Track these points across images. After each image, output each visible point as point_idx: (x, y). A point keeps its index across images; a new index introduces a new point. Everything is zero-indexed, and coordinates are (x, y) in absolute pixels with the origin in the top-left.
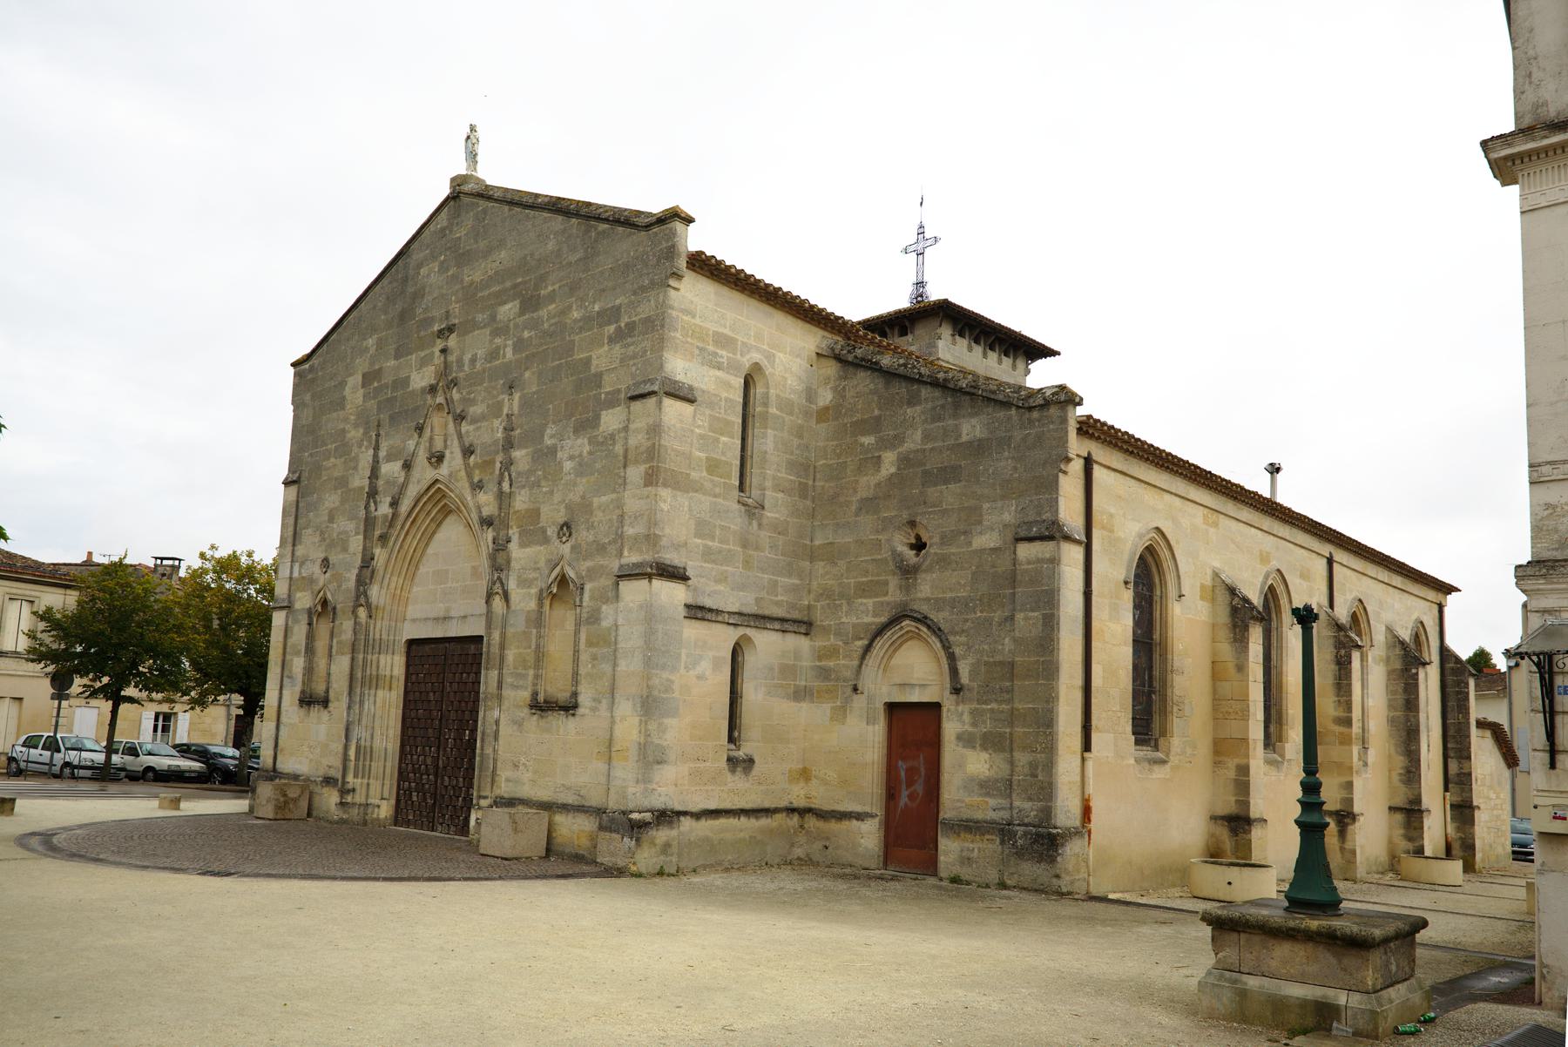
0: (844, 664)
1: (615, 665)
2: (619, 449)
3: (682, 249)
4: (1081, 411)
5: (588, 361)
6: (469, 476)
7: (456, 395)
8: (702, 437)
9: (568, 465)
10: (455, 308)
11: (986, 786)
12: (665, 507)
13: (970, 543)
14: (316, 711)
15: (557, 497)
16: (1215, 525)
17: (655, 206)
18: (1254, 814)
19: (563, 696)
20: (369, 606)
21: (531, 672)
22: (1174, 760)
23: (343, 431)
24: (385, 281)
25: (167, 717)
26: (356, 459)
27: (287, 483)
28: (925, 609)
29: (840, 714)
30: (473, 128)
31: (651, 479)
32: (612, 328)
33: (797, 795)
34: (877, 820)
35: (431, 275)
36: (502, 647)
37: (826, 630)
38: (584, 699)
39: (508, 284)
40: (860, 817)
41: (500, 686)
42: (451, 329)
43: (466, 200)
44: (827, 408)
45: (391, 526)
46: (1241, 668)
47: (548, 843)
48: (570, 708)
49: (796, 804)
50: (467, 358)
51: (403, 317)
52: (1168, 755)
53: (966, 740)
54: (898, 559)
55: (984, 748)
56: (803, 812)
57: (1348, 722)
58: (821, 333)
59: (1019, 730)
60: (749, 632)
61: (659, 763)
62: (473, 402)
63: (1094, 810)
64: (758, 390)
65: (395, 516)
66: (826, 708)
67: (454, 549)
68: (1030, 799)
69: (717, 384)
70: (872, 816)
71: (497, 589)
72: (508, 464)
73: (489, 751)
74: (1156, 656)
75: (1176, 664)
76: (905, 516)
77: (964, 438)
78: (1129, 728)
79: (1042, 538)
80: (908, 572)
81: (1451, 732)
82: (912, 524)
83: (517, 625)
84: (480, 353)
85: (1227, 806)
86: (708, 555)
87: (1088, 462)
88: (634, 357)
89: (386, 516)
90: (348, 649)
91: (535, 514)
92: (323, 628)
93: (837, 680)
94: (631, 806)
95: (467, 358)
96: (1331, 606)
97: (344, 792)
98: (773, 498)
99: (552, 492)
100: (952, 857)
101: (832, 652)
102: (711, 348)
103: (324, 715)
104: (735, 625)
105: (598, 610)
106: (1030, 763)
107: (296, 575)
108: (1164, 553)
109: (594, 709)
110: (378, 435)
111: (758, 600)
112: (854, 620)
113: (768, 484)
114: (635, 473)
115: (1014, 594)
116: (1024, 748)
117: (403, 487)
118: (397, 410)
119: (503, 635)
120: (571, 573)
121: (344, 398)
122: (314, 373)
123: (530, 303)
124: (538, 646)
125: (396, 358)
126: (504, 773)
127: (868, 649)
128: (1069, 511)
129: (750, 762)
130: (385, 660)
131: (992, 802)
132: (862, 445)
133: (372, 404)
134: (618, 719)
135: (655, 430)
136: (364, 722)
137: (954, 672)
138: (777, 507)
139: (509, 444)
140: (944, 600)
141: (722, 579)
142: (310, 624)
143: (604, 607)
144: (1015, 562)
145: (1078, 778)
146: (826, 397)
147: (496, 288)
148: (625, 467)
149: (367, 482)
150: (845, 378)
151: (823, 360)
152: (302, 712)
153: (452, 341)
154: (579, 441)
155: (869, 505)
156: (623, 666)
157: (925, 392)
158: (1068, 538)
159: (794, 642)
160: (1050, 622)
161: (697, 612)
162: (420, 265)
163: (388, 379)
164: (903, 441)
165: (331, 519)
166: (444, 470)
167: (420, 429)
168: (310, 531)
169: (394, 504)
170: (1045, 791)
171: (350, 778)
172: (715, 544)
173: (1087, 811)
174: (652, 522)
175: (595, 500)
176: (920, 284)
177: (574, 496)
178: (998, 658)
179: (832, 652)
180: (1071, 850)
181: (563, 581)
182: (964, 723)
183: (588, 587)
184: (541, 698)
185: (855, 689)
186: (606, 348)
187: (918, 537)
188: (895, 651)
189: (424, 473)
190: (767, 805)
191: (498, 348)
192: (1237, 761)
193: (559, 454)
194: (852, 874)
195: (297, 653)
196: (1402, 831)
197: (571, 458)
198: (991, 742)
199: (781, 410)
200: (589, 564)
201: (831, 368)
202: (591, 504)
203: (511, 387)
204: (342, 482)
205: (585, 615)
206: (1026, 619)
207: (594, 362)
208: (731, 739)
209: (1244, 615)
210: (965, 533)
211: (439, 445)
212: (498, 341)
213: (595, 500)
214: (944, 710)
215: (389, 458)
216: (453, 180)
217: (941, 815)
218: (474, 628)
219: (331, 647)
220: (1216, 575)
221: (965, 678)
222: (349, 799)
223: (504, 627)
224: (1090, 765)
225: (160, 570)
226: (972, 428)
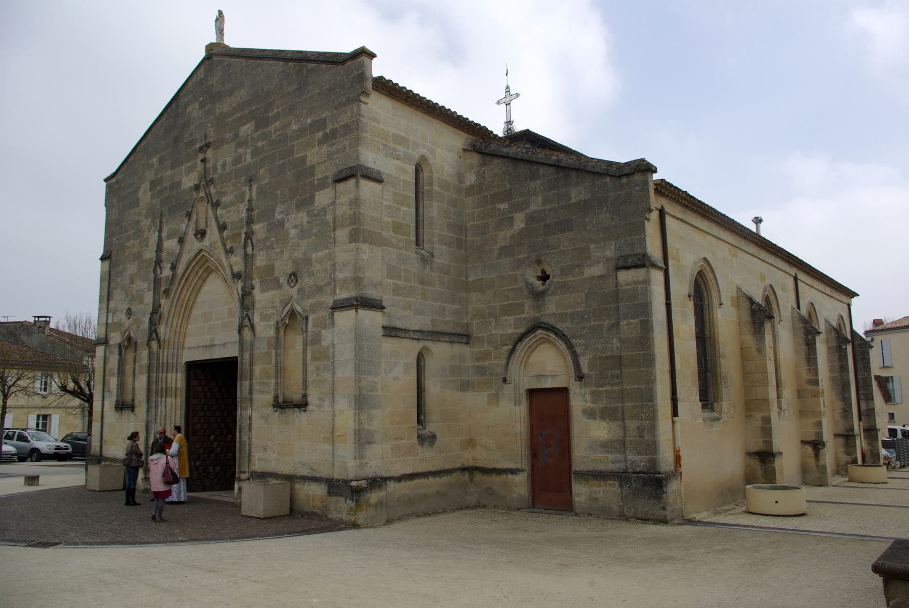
0: (496, 363)
1: (334, 373)
2: (329, 217)
3: (368, 75)
4: (656, 177)
5: (304, 158)
6: (224, 245)
7: (213, 190)
8: (388, 207)
9: (293, 232)
10: (211, 132)
11: (606, 446)
12: (365, 257)
14: (126, 414)
15: (286, 255)
16: (735, 256)
17: (347, 47)
18: (775, 450)
19: (297, 398)
21: (273, 381)
22: (724, 417)
23: (139, 221)
24: (163, 119)
25: (45, 417)
26: (147, 240)
27: (103, 259)
28: (552, 321)
29: (495, 399)
30: (220, 13)
31: (355, 237)
32: (320, 134)
33: (468, 458)
34: (526, 473)
35: (194, 111)
36: (251, 364)
37: (481, 340)
38: (312, 399)
39: (246, 111)
40: (513, 472)
41: (251, 393)
42: (208, 145)
43: (216, 59)
44: (472, 187)
45: (171, 283)
46: (761, 350)
47: (291, 504)
49: (466, 465)
50: (219, 165)
51: (176, 140)
52: (720, 412)
53: (590, 414)
54: (529, 285)
55: (603, 418)
56: (471, 470)
57: (816, 382)
58: (465, 135)
59: (628, 404)
60: (429, 344)
61: (370, 443)
62: (224, 194)
63: (682, 458)
64: (426, 174)
65: (174, 276)
66: (485, 394)
67: (217, 295)
68: (639, 454)
69: (397, 170)
70: (522, 470)
71: (246, 323)
72: (249, 236)
73: (245, 439)
74: (708, 347)
75: (721, 351)
76: (533, 256)
77: (574, 200)
78: (698, 398)
79: (636, 267)
80: (538, 296)
81: (861, 384)
82: (539, 262)
83: (261, 348)
84: (229, 159)
85: (757, 444)
86: (396, 290)
87: (662, 213)
88: (338, 152)
89: (168, 277)
90: (145, 370)
91: (270, 269)
92: (130, 356)
93: (491, 374)
94: (351, 476)
95: (219, 165)
96: (799, 307)
98: (439, 248)
99: (282, 252)
100: (583, 498)
101: (486, 356)
102: (391, 145)
103: (132, 416)
104: (418, 339)
105: (319, 334)
106: (638, 428)
107: (110, 321)
108: (709, 275)
109: (319, 406)
110: (161, 222)
111: (433, 321)
112: (501, 332)
113: (436, 239)
114: (342, 234)
115: (618, 307)
116: (633, 417)
117: (179, 256)
118: (174, 204)
119: (252, 355)
120: (299, 309)
121: (138, 199)
122: (119, 186)
123: (262, 122)
124: (277, 363)
125: (172, 169)
126: (257, 455)
127: (512, 351)
128: (653, 248)
129: (433, 437)
130: (171, 377)
131: (611, 457)
132: (499, 210)
133: (157, 201)
134: (337, 413)
135: (356, 202)
136: (158, 421)
137: (577, 365)
138: (442, 255)
139: (250, 221)
140: (566, 314)
141: (408, 307)
142: (120, 354)
143: (324, 332)
144: (617, 284)
145: (671, 436)
146: (471, 179)
147: (238, 115)
148: (334, 230)
149: (154, 254)
151: (468, 154)
152: (117, 414)
153: (209, 154)
154: (300, 215)
155: (506, 251)
156: (339, 373)
157: (542, 170)
158: (654, 266)
159: (458, 349)
160: (646, 326)
161: (391, 331)
162: (186, 107)
163: (167, 184)
165: (132, 282)
166: (206, 242)
167: (189, 215)
168: (118, 291)
169: (174, 268)
170: (652, 447)
172: (401, 283)
173: (678, 459)
174: (357, 269)
175: (314, 255)
176: (509, 123)
177: (298, 254)
178: (609, 354)
179: (486, 356)
180: (673, 487)
181: (293, 314)
182: (586, 401)
183: (311, 318)
184: (280, 400)
185: (505, 380)
186: (317, 148)
187: (543, 272)
188: (532, 351)
189: (193, 245)
190: (447, 467)
191: (241, 155)
192: (761, 414)
193: (286, 225)
194: (505, 506)
195: (113, 375)
196: (843, 449)
197: (295, 227)
198: (607, 414)
199: (440, 187)
200: (311, 301)
201: (475, 159)
202: (310, 259)
203: (250, 181)
204: (138, 256)
205: (309, 338)
207: (309, 159)
208: (419, 422)
209: (760, 314)
210: (578, 266)
211: (202, 226)
212: (240, 150)
213: (314, 255)
214: (571, 394)
215: (169, 237)
216: (207, 47)
217: (574, 468)
218: (231, 351)
219: (134, 369)
220: (739, 289)
221: (585, 370)
223: (252, 350)
224: (678, 426)
225: (38, 324)
226: (578, 193)
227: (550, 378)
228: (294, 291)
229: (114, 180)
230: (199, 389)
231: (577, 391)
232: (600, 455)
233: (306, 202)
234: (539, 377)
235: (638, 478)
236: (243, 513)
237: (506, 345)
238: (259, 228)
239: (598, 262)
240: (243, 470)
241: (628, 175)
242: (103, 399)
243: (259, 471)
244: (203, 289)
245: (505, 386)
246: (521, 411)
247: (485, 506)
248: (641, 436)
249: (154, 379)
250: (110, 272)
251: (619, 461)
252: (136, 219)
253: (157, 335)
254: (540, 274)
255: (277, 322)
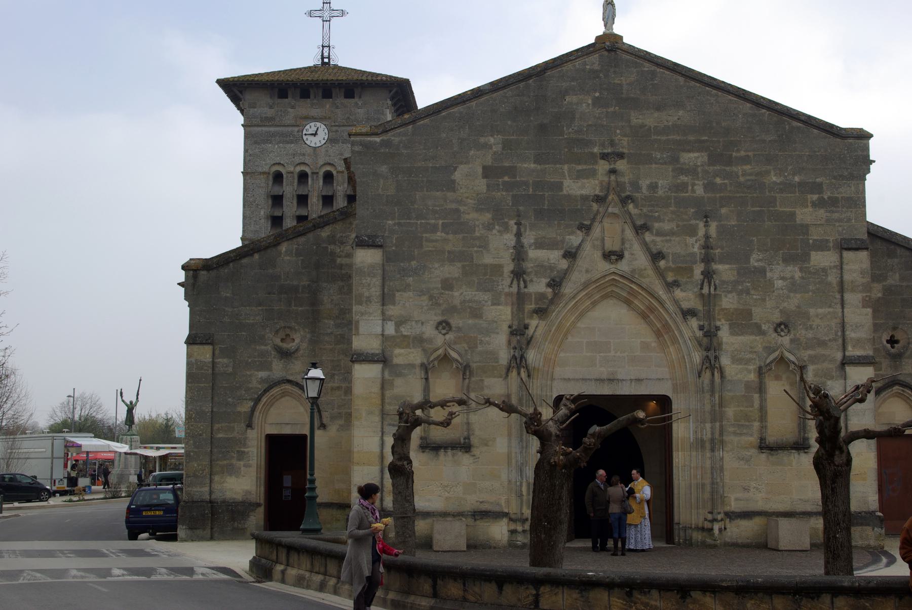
9: (779, 283)
20: (527, 367)
32: (815, 197)
157: (899, 251)
197: (783, 278)
228: (786, 340)
243: (737, 510)
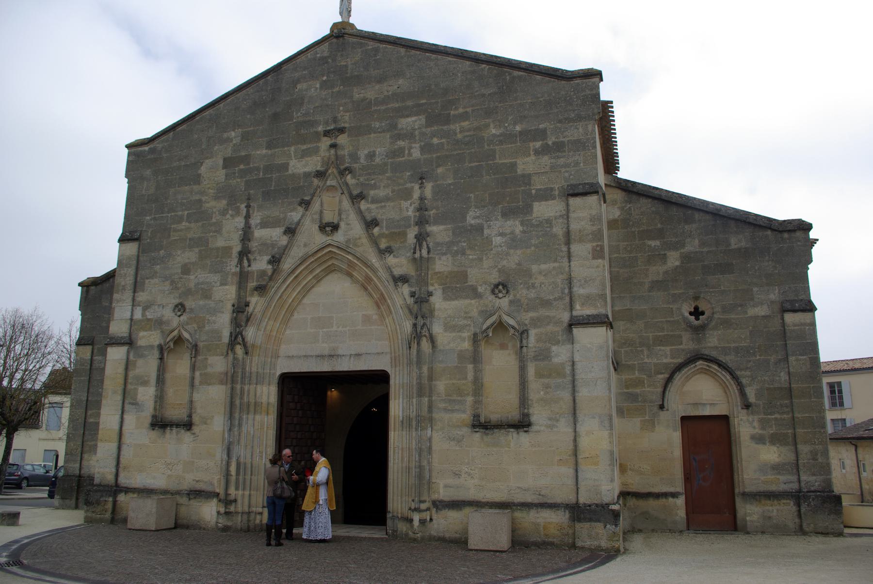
5: (514, 165)
9: (497, 240)
11: (777, 468)
13: (746, 312)
15: (486, 263)
20: (245, 345)
24: (250, 90)
27: (122, 240)
28: (714, 354)
29: (650, 425)
37: (631, 368)
38: (538, 415)
40: (674, 495)
48: (522, 424)
53: (759, 439)
66: (637, 421)
68: (814, 475)
76: (691, 292)
77: (733, 247)
82: (696, 298)
97: (228, 502)
100: (755, 517)
101: (639, 383)
106: (811, 452)
112: (655, 361)
125: (269, 146)
131: (782, 478)
132: (650, 246)
136: (243, 442)
142: (161, 359)
144: (783, 324)
150: (630, 202)
153: (342, 139)
155: (657, 285)
157: (697, 216)
162: (295, 82)
164: (683, 246)
166: (339, 237)
171: (232, 491)
178: (776, 385)
179: (639, 383)
182: (754, 428)
183: (533, 333)
185: (662, 407)
187: (696, 308)
193: (486, 232)
195: (145, 383)
197: (502, 234)
198: (775, 439)
206: (797, 360)
210: (741, 306)
212: (401, 143)
221: (752, 399)
222: (232, 509)
227: (708, 407)
229: (146, 148)
230: (292, 405)
231: (744, 418)
232: (770, 477)
233: (519, 209)
234: (696, 405)
235: (817, 496)
236: (470, 547)
237: (662, 373)
238: (439, 232)
239: (762, 304)
240: (422, 499)
241: (789, 231)
242: (123, 413)
243: (446, 499)
244: (315, 290)
245: (661, 413)
246: (677, 436)
247: (640, 531)
248: (815, 459)
249: (238, 392)
250: (138, 256)
251: (791, 482)
252: (197, 197)
253: (243, 339)
254: (692, 310)
255: (475, 335)
